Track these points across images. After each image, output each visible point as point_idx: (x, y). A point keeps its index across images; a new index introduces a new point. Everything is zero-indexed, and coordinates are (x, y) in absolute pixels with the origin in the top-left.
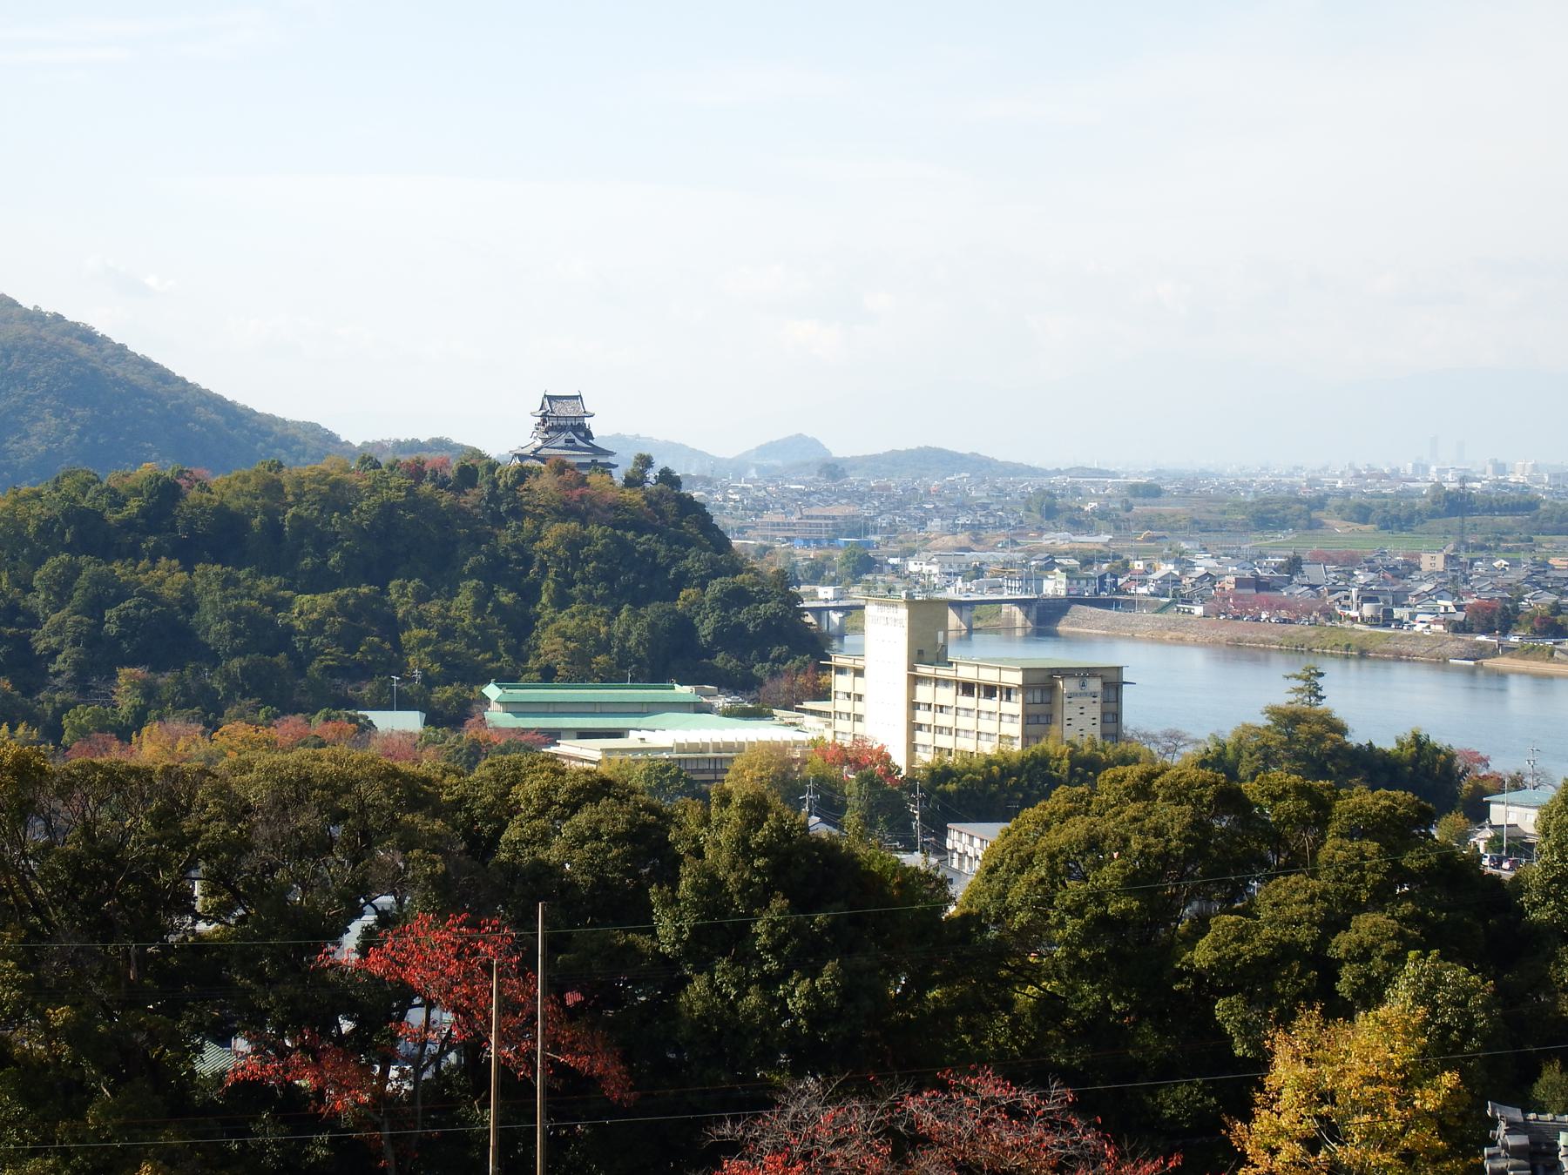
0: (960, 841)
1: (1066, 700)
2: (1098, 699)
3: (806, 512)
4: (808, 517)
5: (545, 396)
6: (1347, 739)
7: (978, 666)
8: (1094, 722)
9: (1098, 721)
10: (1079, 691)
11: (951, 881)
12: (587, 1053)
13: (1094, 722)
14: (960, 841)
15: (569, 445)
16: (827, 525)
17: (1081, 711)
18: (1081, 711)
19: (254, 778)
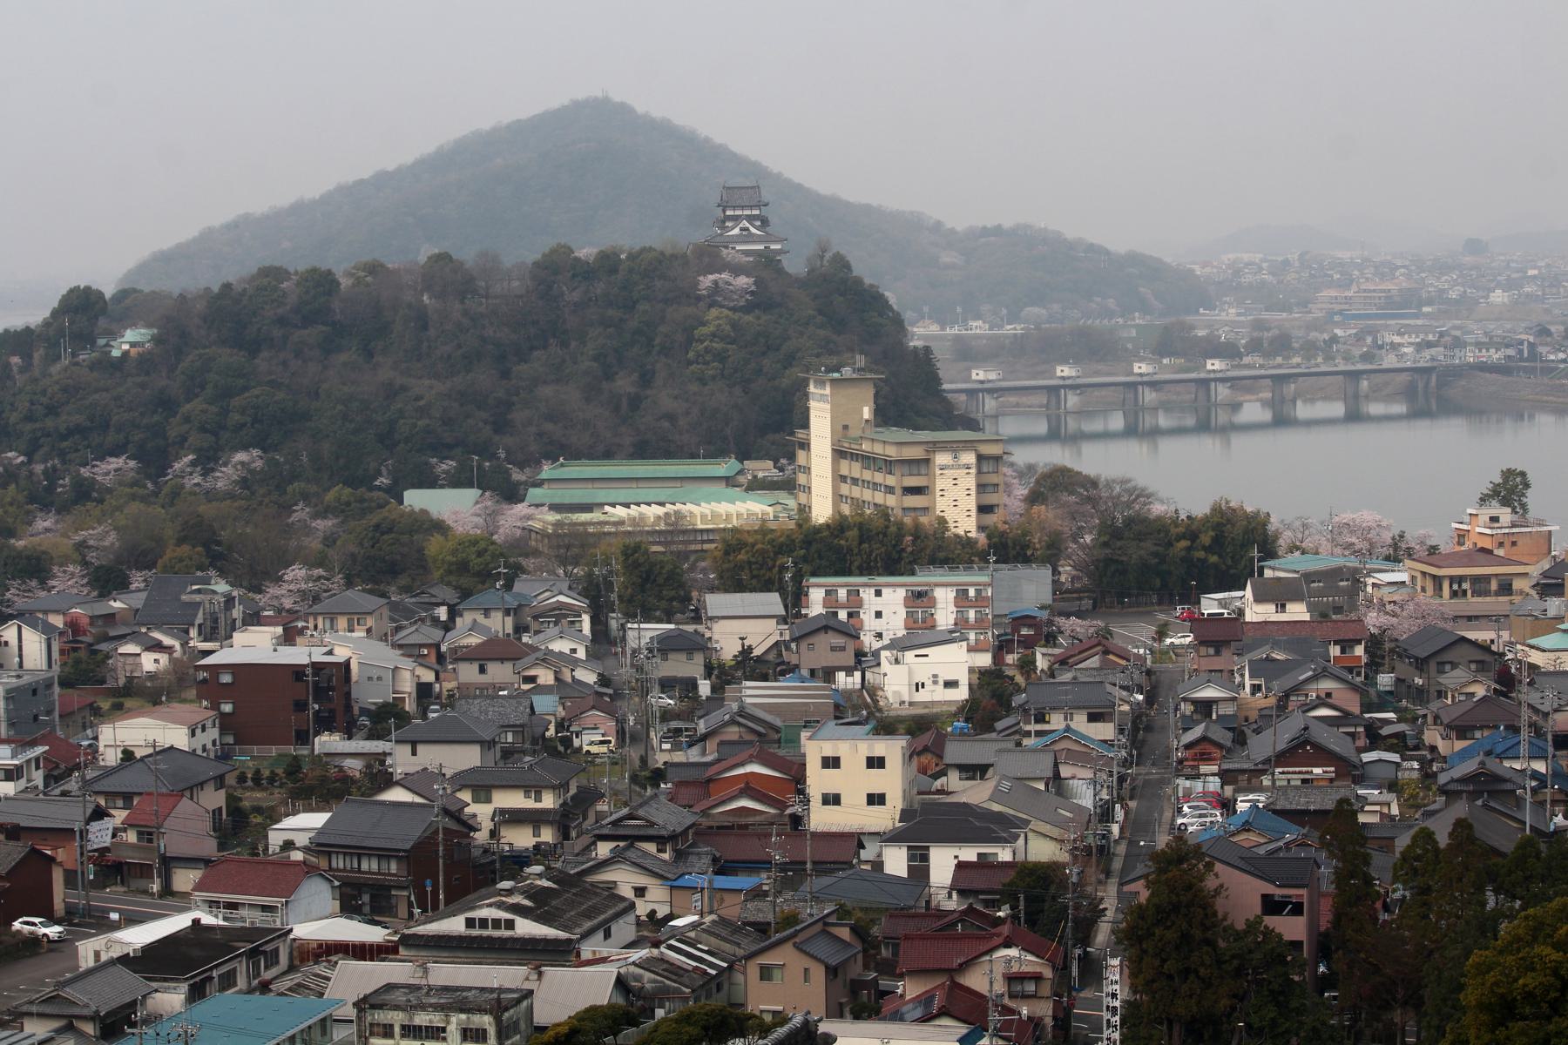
0: (542, 542)
1: (938, 472)
2: (973, 471)
3: (1363, 287)
4: (1365, 291)
5: (724, 187)
6: (1040, 471)
7: (873, 440)
8: (968, 492)
9: (973, 492)
10: (951, 462)
11: (1247, 920)
12: (89, 547)
13: (968, 492)
14: (542, 542)
15: (744, 233)
16: (1380, 298)
17: (954, 482)
18: (954, 482)
19: (214, 972)
